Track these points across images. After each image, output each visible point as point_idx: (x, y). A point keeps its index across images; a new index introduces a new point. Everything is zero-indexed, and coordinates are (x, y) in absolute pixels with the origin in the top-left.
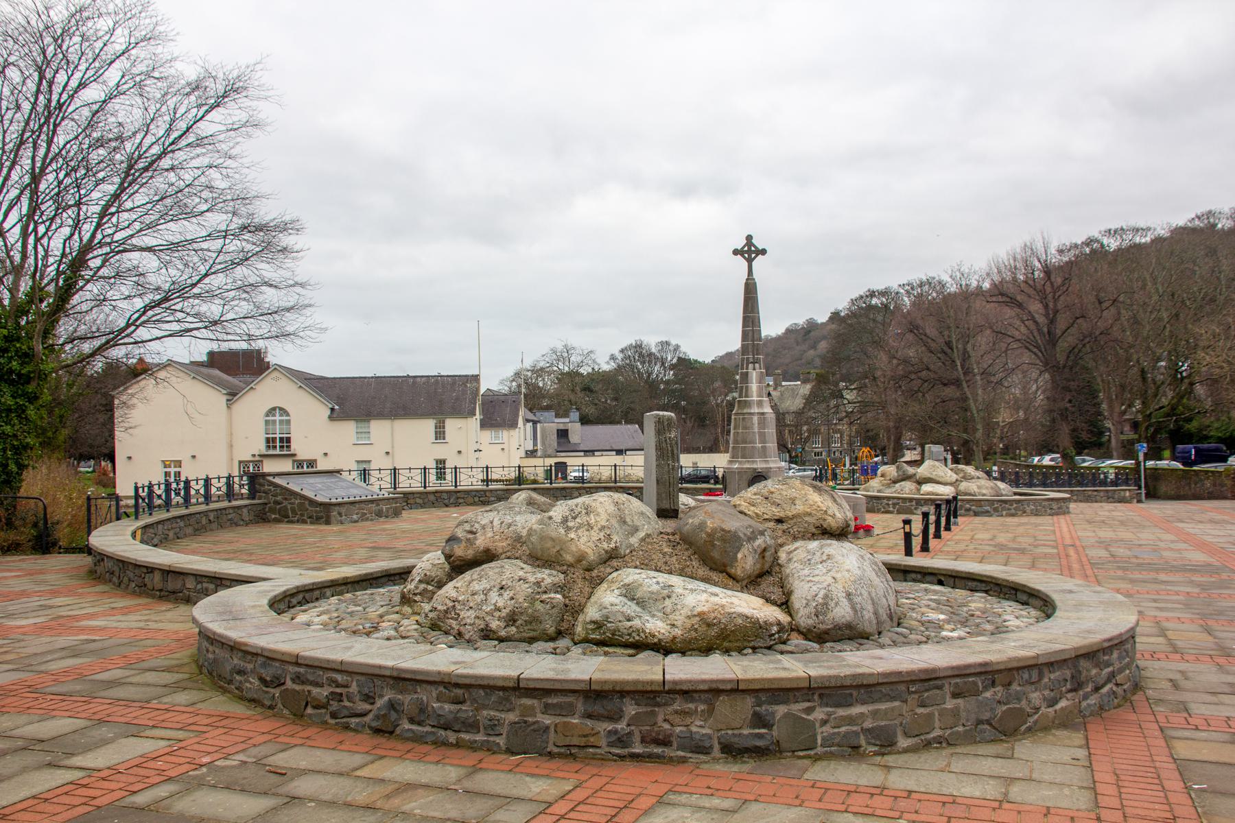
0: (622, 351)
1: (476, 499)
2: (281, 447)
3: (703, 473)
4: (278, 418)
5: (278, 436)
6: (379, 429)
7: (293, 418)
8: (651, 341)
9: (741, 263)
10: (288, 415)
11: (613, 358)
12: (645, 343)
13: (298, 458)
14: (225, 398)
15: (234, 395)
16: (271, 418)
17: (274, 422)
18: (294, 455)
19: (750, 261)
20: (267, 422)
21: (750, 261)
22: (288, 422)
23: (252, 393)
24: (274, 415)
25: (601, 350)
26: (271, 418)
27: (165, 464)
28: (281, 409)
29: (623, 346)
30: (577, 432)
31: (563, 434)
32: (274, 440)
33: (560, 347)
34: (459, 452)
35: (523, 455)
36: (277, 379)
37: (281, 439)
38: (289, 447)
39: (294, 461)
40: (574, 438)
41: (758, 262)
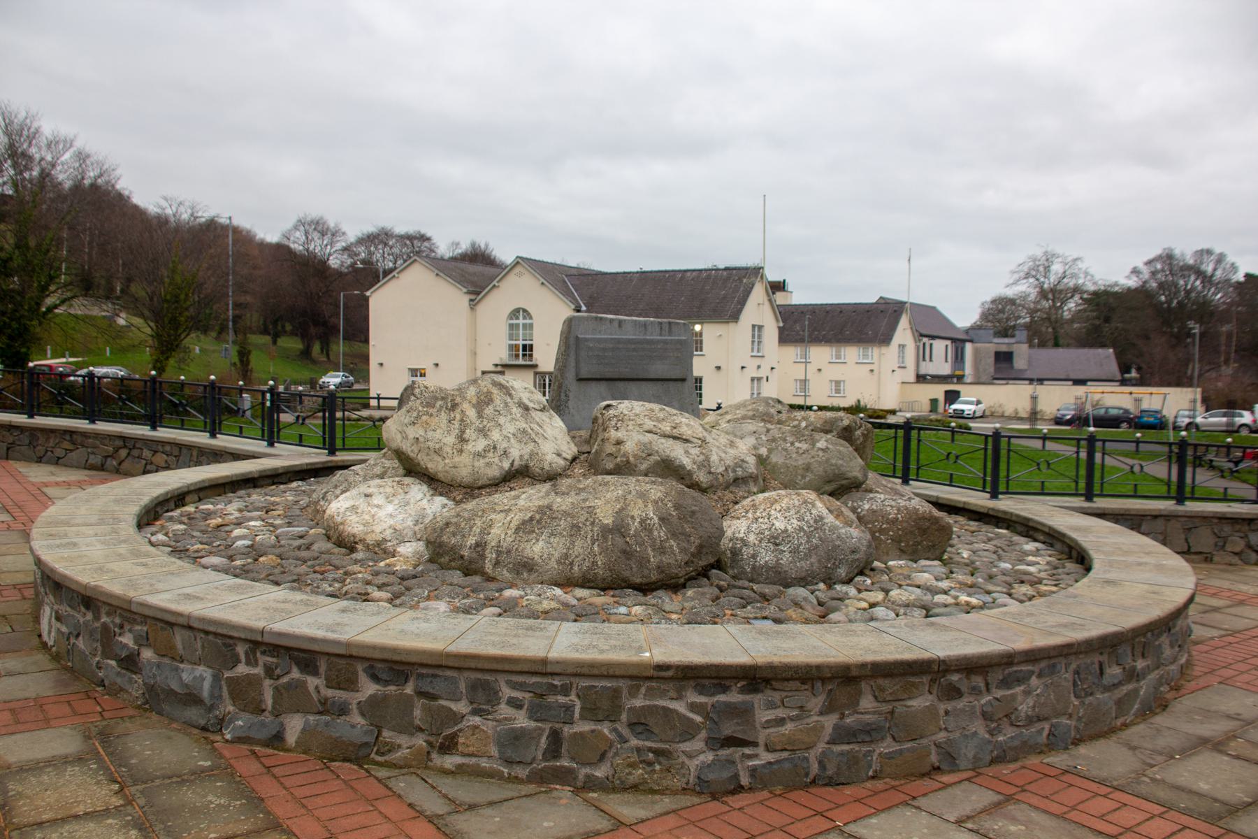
0: (1149, 263)
2: (524, 355)
3: (1113, 412)
4: (521, 321)
5: (521, 343)
6: (820, 354)
7: (535, 321)
8: (1186, 250)
10: (531, 318)
11: (1135, 271)
12: (1177, 252)
13: (540, 369)
14: (466, 298)
15: (478, 294)
16: (515, 322)
17: (518, 325)
18: (536, 366)
20: (511, 326)
22: (531, 325)
23: (495, 291)
24: (517, 318)
25: (1114, 267)
26: (515, 322)
27: (414, 372)
28: (525, 311)
29: (1151, 256)
30: (1023, 354)
32: (517, 346)
33: (1039, 252)
34: (718, 368)
35: (912, 378)
36: (520, 275)
37: (524, 347)
38: (531, 356)
39: (536, 373)
40: (1019, 363)
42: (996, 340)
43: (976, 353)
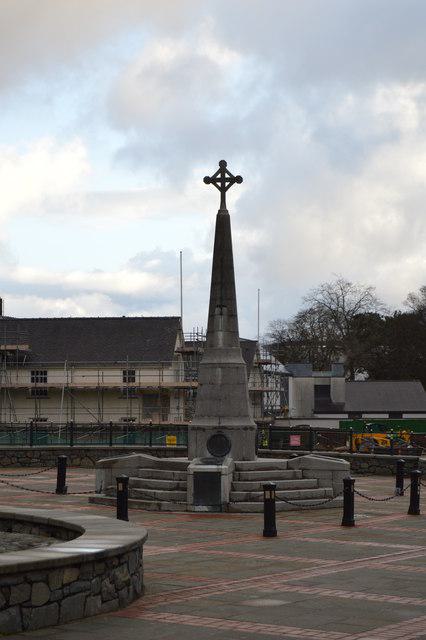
1: (14, 460)
9: (213, 191)
11: (412, 298)
19: (223, 190)
21: (223, 190)
31: (322, 391)
41: (234, 193)
42: (315, 374)
43: (296, 385)
